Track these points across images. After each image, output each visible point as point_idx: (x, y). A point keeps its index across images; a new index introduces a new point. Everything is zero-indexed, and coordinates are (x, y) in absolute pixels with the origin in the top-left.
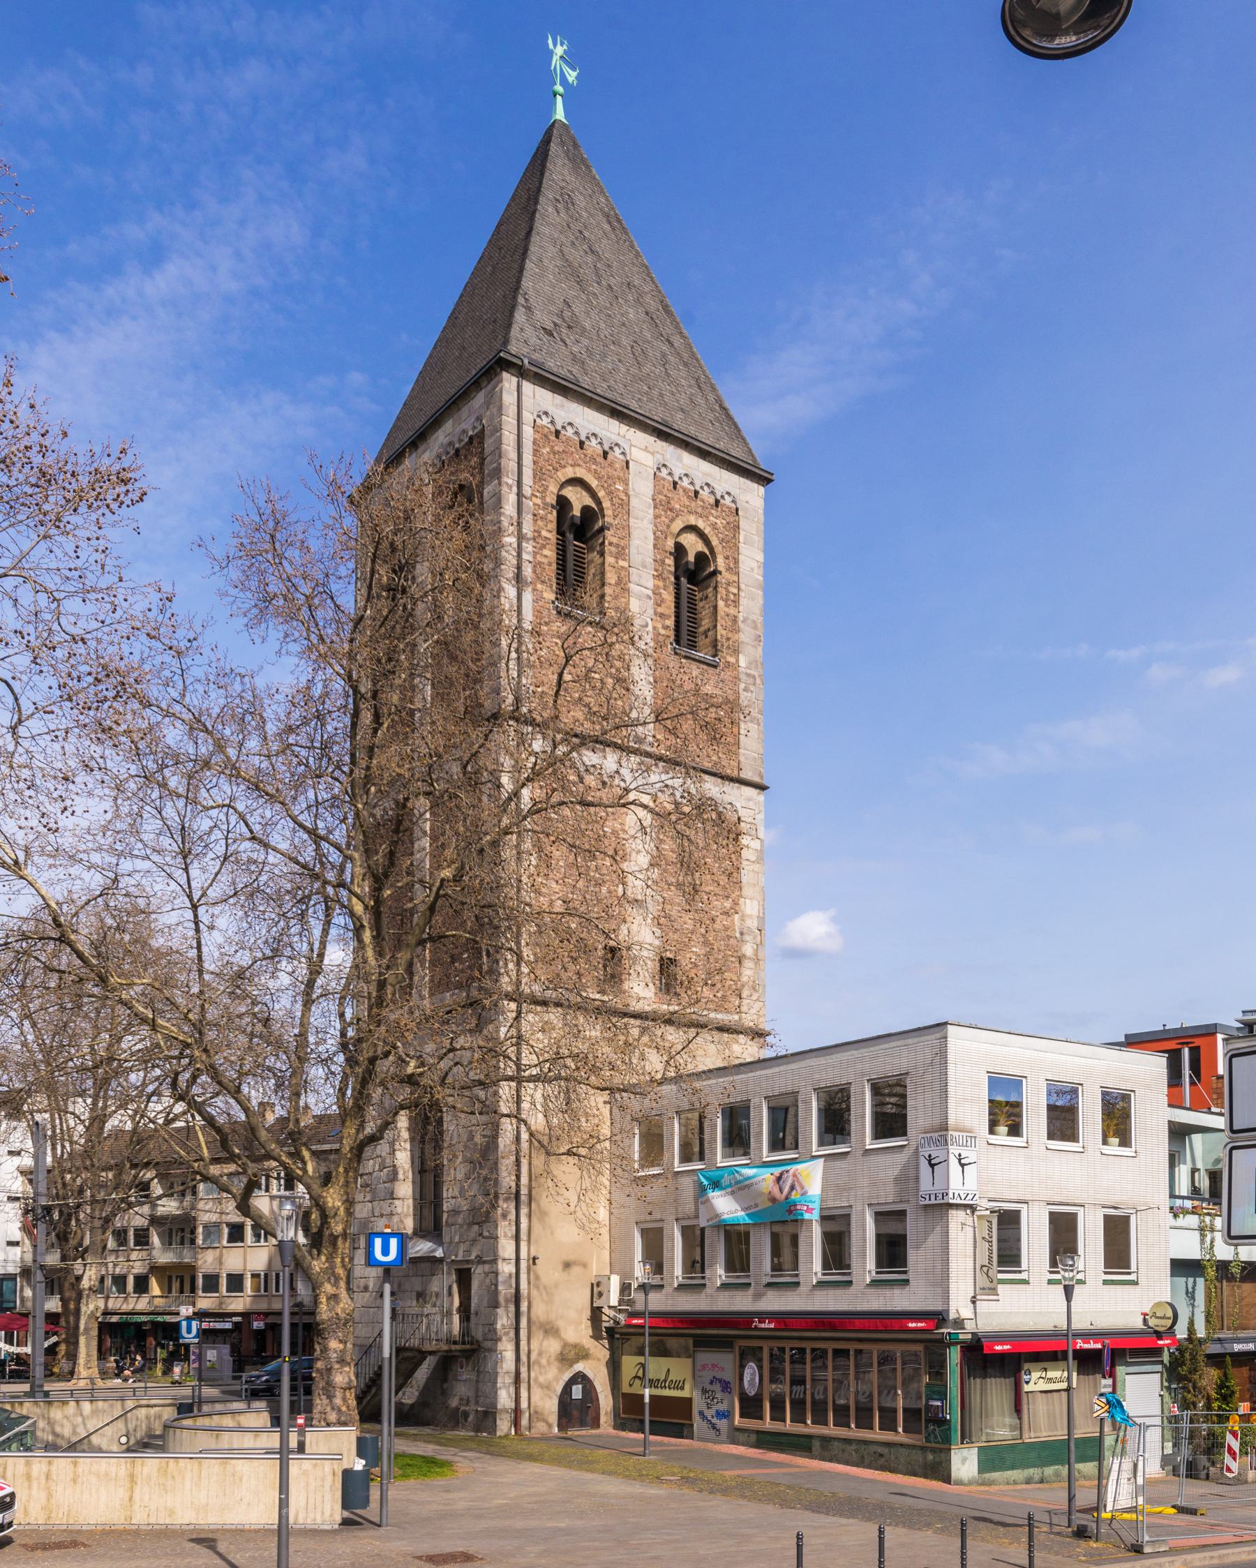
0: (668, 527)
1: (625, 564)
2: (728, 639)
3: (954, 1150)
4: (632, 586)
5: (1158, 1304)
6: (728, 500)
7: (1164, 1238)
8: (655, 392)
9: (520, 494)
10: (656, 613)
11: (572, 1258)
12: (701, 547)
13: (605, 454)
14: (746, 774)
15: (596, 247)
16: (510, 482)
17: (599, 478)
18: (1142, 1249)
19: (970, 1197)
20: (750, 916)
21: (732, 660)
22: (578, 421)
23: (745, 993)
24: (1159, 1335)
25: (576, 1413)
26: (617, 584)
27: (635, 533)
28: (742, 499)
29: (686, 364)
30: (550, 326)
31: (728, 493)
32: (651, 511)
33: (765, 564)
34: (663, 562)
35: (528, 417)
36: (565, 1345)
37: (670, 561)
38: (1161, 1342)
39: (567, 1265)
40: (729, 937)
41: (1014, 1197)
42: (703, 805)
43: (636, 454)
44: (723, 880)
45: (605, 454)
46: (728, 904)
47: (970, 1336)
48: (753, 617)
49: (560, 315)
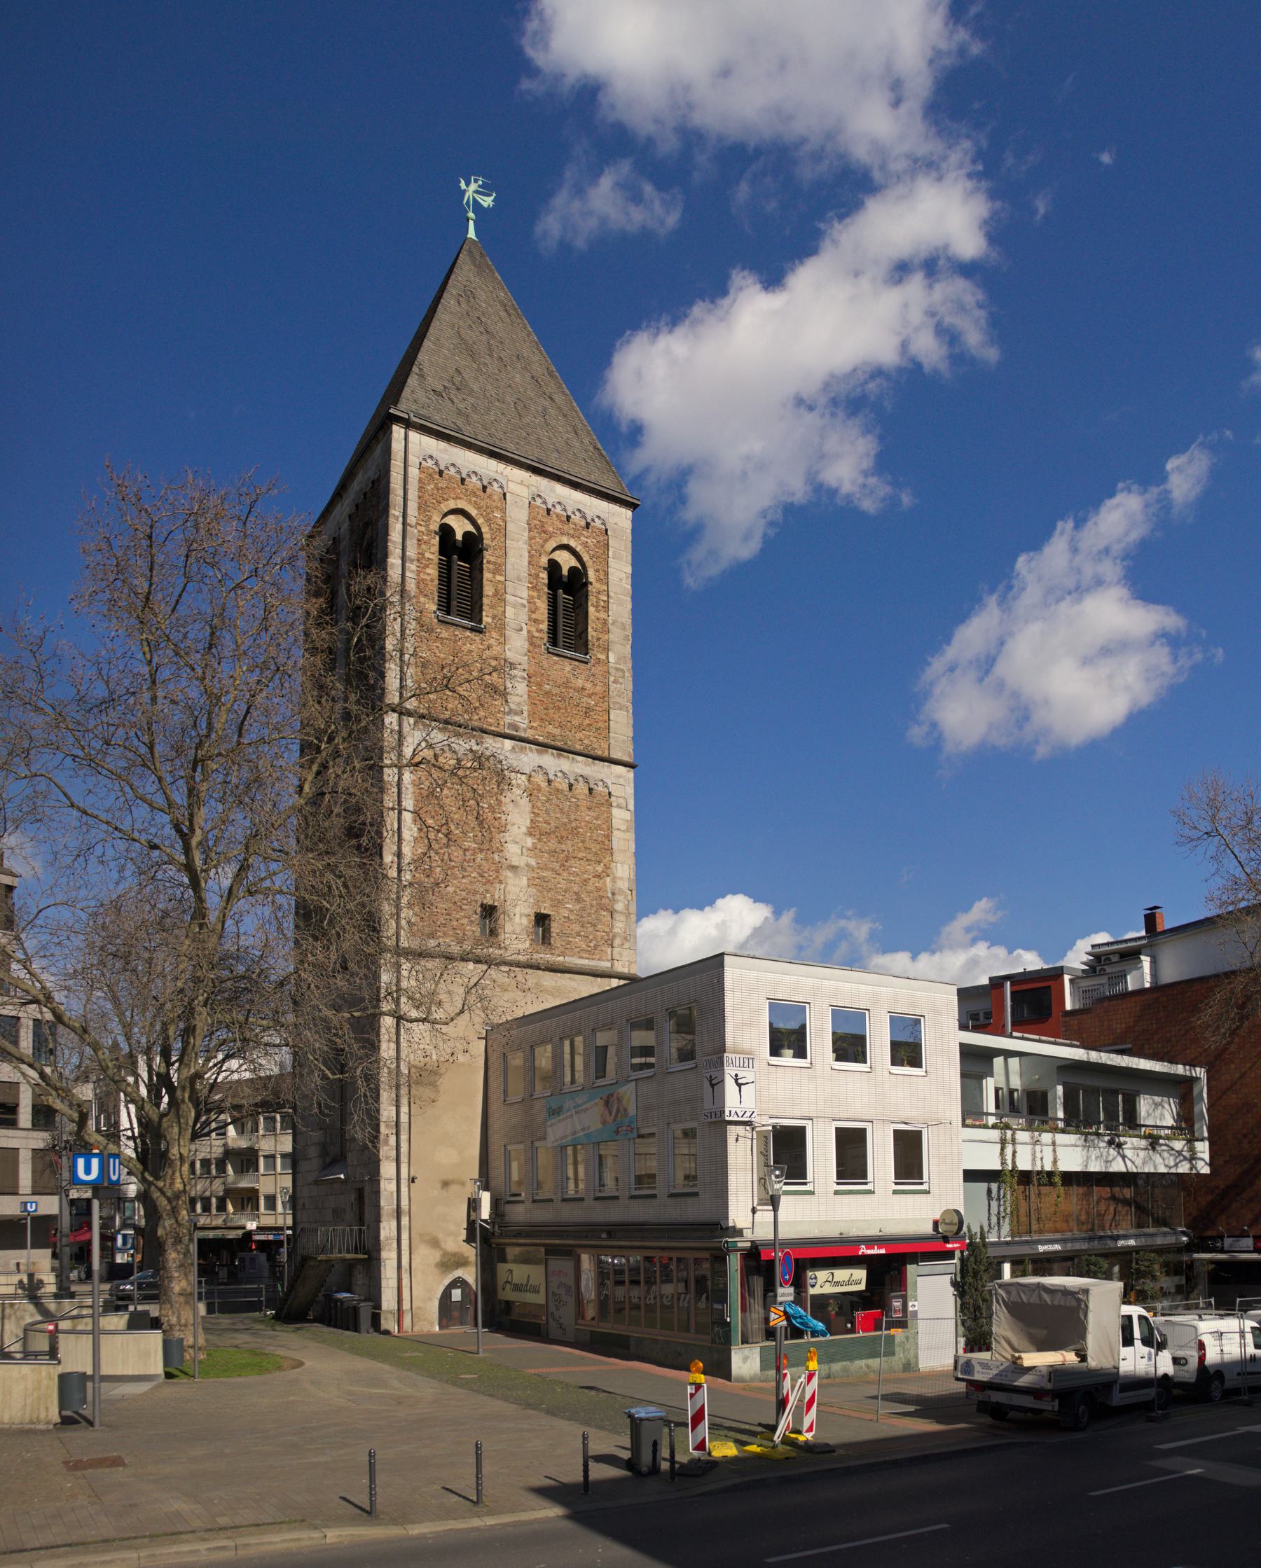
0: (542, 546)
1: (502, 579)
2: (599, 639)
3: (729, 1072)
4: (508, 596)
5: (947, 1211)
6: (598, 522)
7: (956, 1150)
8: (533, 438)
9: (404, 524)
10: (530, 619)
11: (450, 1177)
12: (574, 562)
13: (484, 488)
14: (616, 755)
15: (491, 328)
16: (397, 513)
17: (478, 508)
18: (934, 1161)
19: (748, 1114)
20: (621, 878)
21: (603, 657)
22: (459, 462)
23: (617, 942)
24: (946, 1239)
25: (456, 1314)
26: (494, 595)
27: (510, 552)
28: (611, 521)
29: (565, 416)
30: (439, 388)
31: (599, 517)
32: (526, 534)
33: (633, 575)
34: (537, 576)
35: (413, 460)
36: (445, 1254)
37: (544, 575)
38: (949, 1246)
39: (446, 1184)
40: (601, 897)
41: (797, 1114)
42: (480, 759)
43: (512, 487)
44: (595, 847)
45: (484, 488)
46: (600, 868)
47: (749, 1244)
48: (623, 620)
49: (451, 381)
